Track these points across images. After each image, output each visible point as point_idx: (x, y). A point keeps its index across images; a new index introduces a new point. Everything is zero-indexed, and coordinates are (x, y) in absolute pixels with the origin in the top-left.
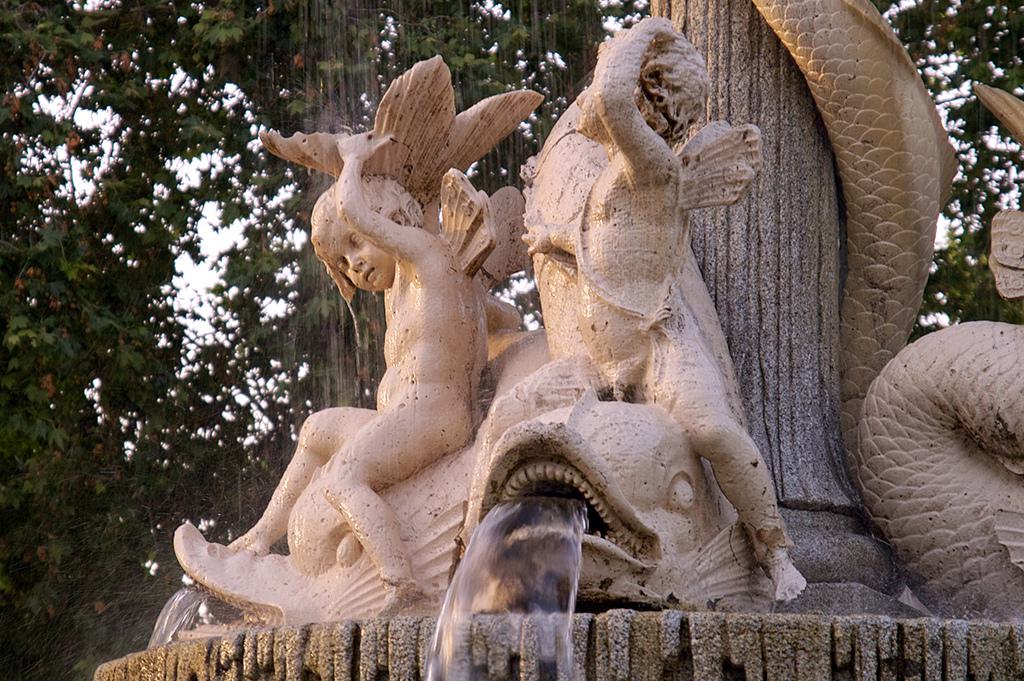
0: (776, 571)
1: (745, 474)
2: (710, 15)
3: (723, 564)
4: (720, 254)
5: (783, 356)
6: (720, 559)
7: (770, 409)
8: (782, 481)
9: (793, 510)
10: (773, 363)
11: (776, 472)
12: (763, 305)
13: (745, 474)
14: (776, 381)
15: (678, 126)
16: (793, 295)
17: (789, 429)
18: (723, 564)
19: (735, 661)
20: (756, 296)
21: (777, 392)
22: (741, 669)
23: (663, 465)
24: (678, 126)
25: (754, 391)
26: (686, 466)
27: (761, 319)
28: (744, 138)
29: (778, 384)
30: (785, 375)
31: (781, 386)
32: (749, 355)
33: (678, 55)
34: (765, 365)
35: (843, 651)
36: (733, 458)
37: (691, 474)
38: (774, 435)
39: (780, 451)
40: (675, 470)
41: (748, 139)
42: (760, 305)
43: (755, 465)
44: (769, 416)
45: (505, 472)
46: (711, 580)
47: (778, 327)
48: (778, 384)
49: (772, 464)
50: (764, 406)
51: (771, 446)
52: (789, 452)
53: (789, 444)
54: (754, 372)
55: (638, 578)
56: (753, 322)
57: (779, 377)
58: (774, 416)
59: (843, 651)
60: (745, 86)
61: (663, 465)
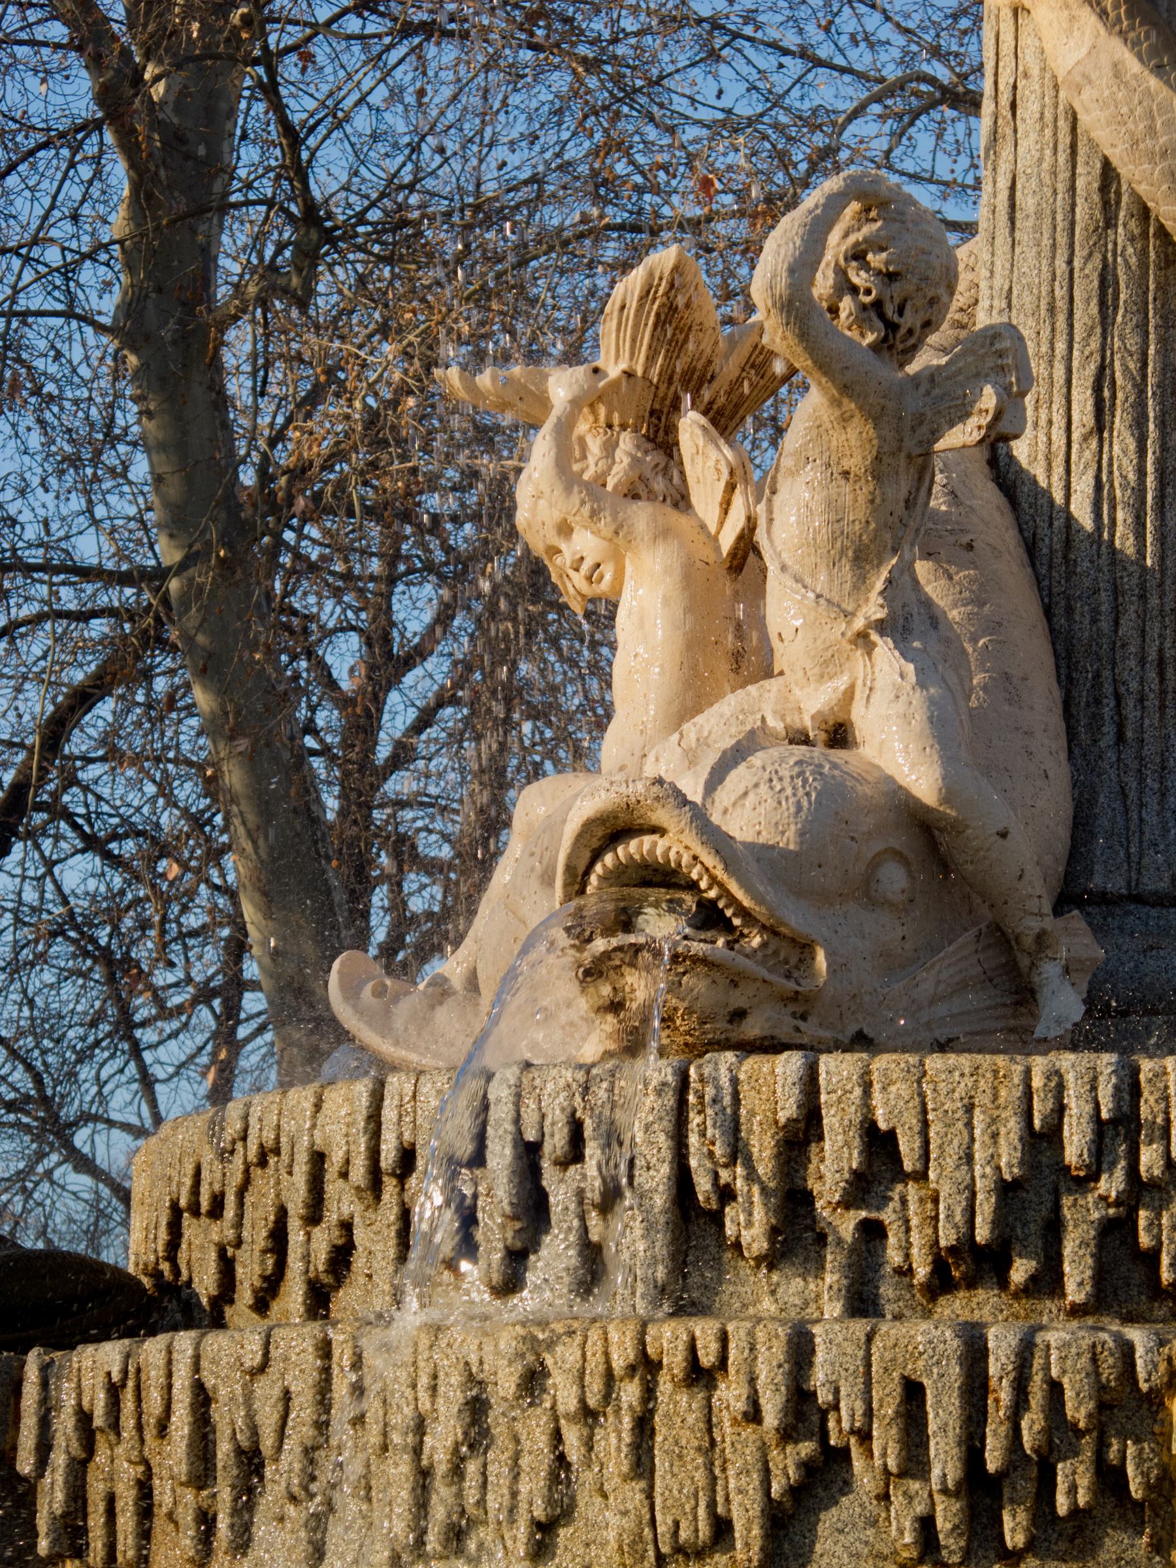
0: (1044, 995)
1: (989, 850)
2: (1045, 166)
3: (962, 987)
4: (1056, 524)
5: (1152, 675)
6: (957, 978)
7: (1129, 754)
8: (1139, 863)
9: (1153, 906)
10: (1134, 685)
11: (1132, 850)
12: (1120, 600)
13: (989, 850)
14: (1139, 714)
15: (903, 331)
16: (1168, 582)
17: (1156, 786)
18: (962, 987)
19: (883, 1125)
20: (1108, 586)
21: (1141, 729)
22: (891, 1134)
23: (853, 839)
24: (903, 331)
25: (1105, 729)
26: (898, 841)
27: (1116, 623)
28: (992, 344)
29: (1142, 718)
30: (1152, 701)
31: (1147, 722)
32: (1097, 675)
33: (897, 225)
34: (1122, 689)
35: (1041, 1109)
36: (967, 827)
37: (906, 852)
38: (1133, 795)
39: (1141, 820)
40: (878, 846)
41: (998, 346)
42: (1116, 599)
43: (1003, 835)
44: (1126, 766)
45: (587, 855)
46: (942, 1010)
47: (1143, 631)
48: (1142, 718)
49: (1127, 839)
50: (1120, 752)
51: (1127, 811)
52: (1155, 820)
53: (1156, 807)
54: (1105, 701)
55: (791, 1008)
56: (1105, 625)
57: (1143, 708)
58: (1135, 765)
59: (1041, 1109)
60: (1095, 269)
61: (853, 839)
